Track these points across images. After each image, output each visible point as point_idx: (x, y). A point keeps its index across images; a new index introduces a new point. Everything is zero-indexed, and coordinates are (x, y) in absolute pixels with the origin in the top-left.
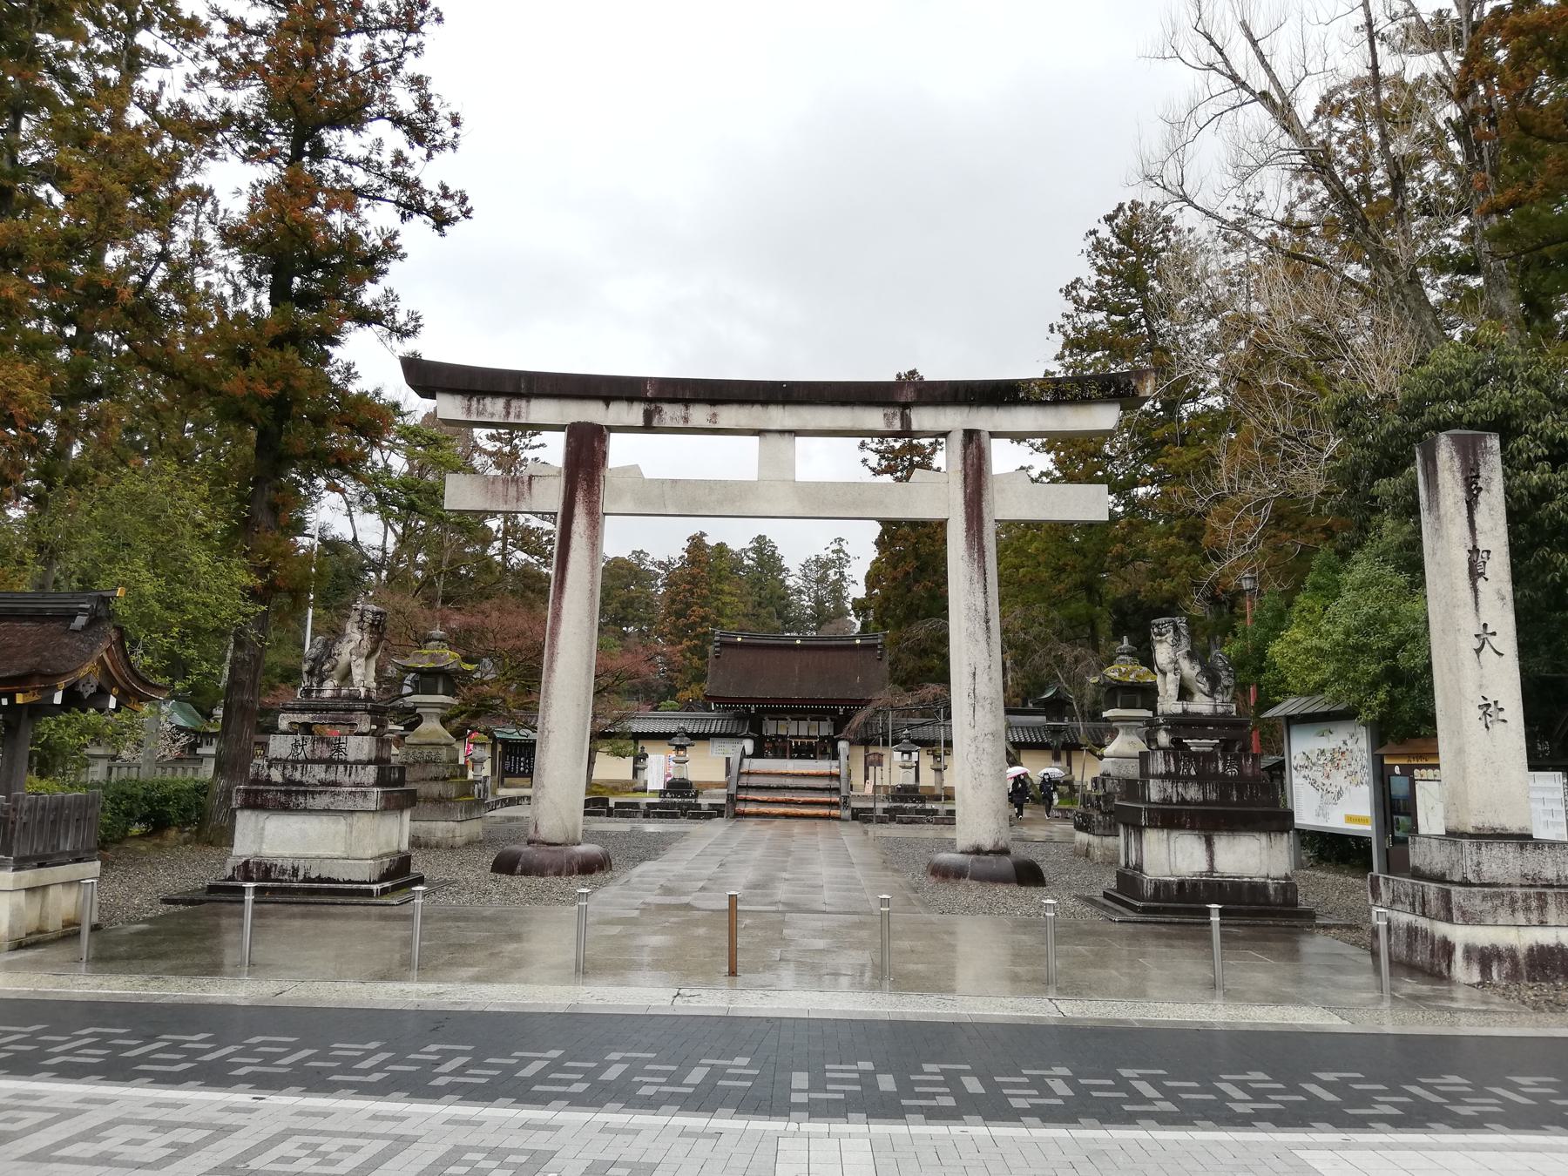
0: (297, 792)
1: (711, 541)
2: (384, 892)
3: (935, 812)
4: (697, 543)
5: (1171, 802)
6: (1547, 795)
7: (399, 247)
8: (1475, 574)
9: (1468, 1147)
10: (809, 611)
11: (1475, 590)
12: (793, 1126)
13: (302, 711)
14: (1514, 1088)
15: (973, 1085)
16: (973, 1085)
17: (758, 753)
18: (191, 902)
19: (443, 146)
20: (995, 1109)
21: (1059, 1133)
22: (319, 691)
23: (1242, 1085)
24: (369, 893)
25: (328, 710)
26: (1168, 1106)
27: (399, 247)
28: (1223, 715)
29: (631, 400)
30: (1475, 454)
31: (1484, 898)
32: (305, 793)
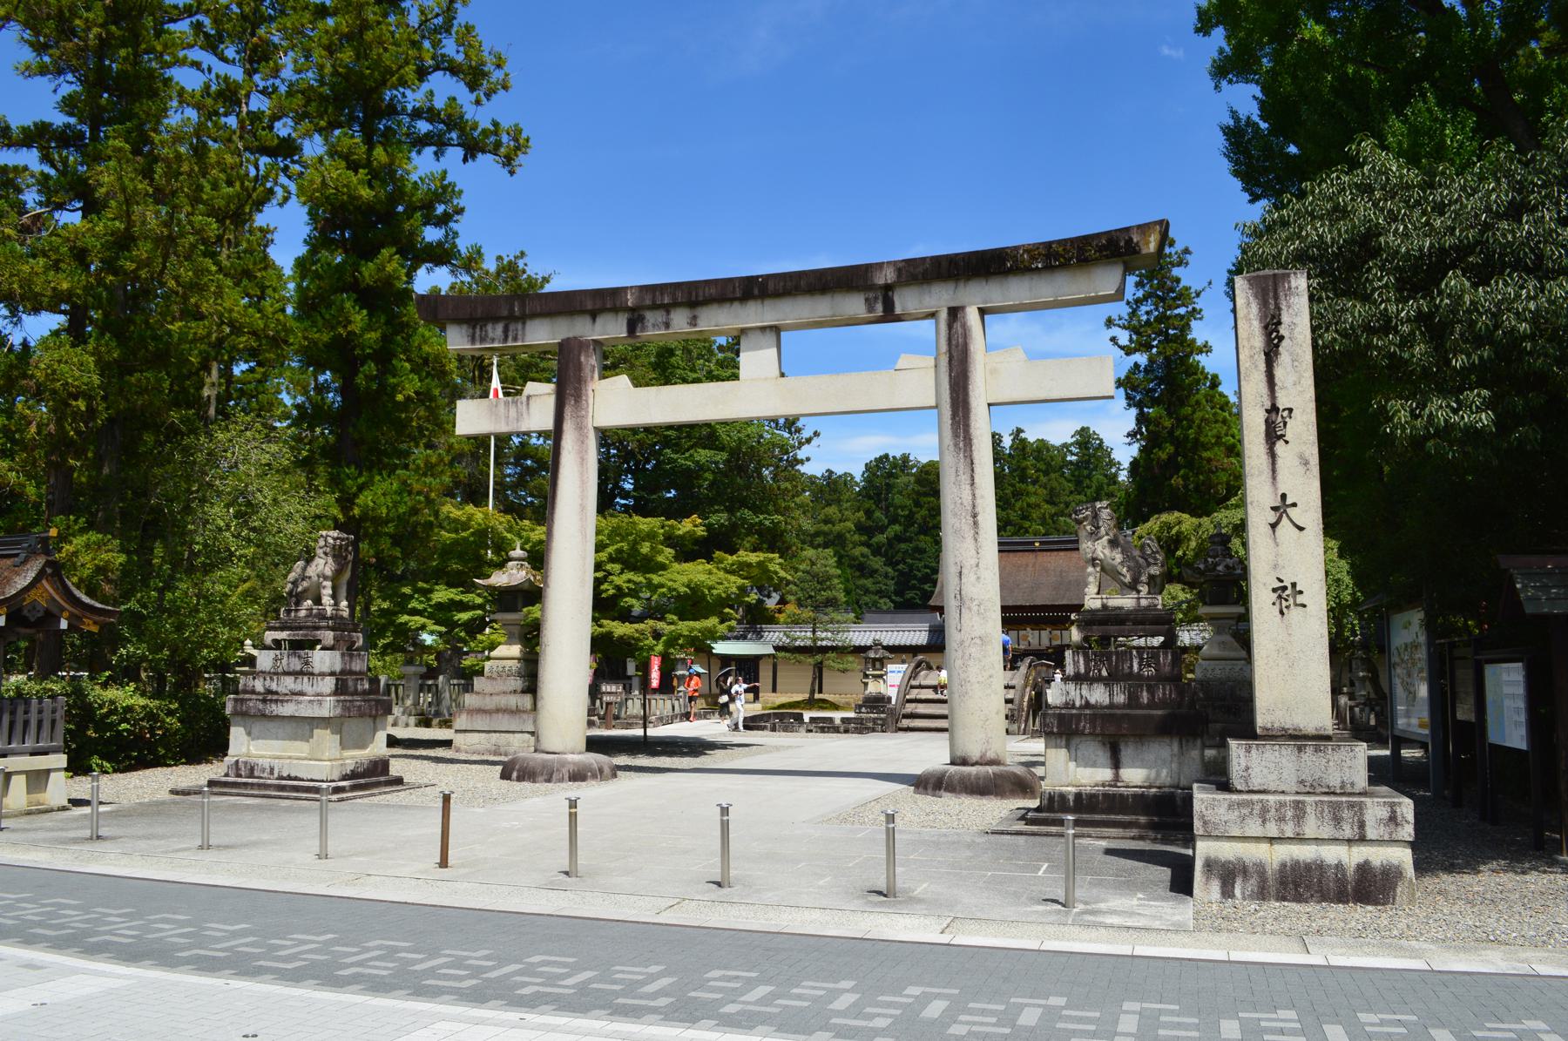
5: (1073, 706)
8: (1273, 435)
11: (1272, 455)
13: (282, 629)
25: (300, 628)
28: (1147, 608)
29: (615, 310)
30: (1276, 298)
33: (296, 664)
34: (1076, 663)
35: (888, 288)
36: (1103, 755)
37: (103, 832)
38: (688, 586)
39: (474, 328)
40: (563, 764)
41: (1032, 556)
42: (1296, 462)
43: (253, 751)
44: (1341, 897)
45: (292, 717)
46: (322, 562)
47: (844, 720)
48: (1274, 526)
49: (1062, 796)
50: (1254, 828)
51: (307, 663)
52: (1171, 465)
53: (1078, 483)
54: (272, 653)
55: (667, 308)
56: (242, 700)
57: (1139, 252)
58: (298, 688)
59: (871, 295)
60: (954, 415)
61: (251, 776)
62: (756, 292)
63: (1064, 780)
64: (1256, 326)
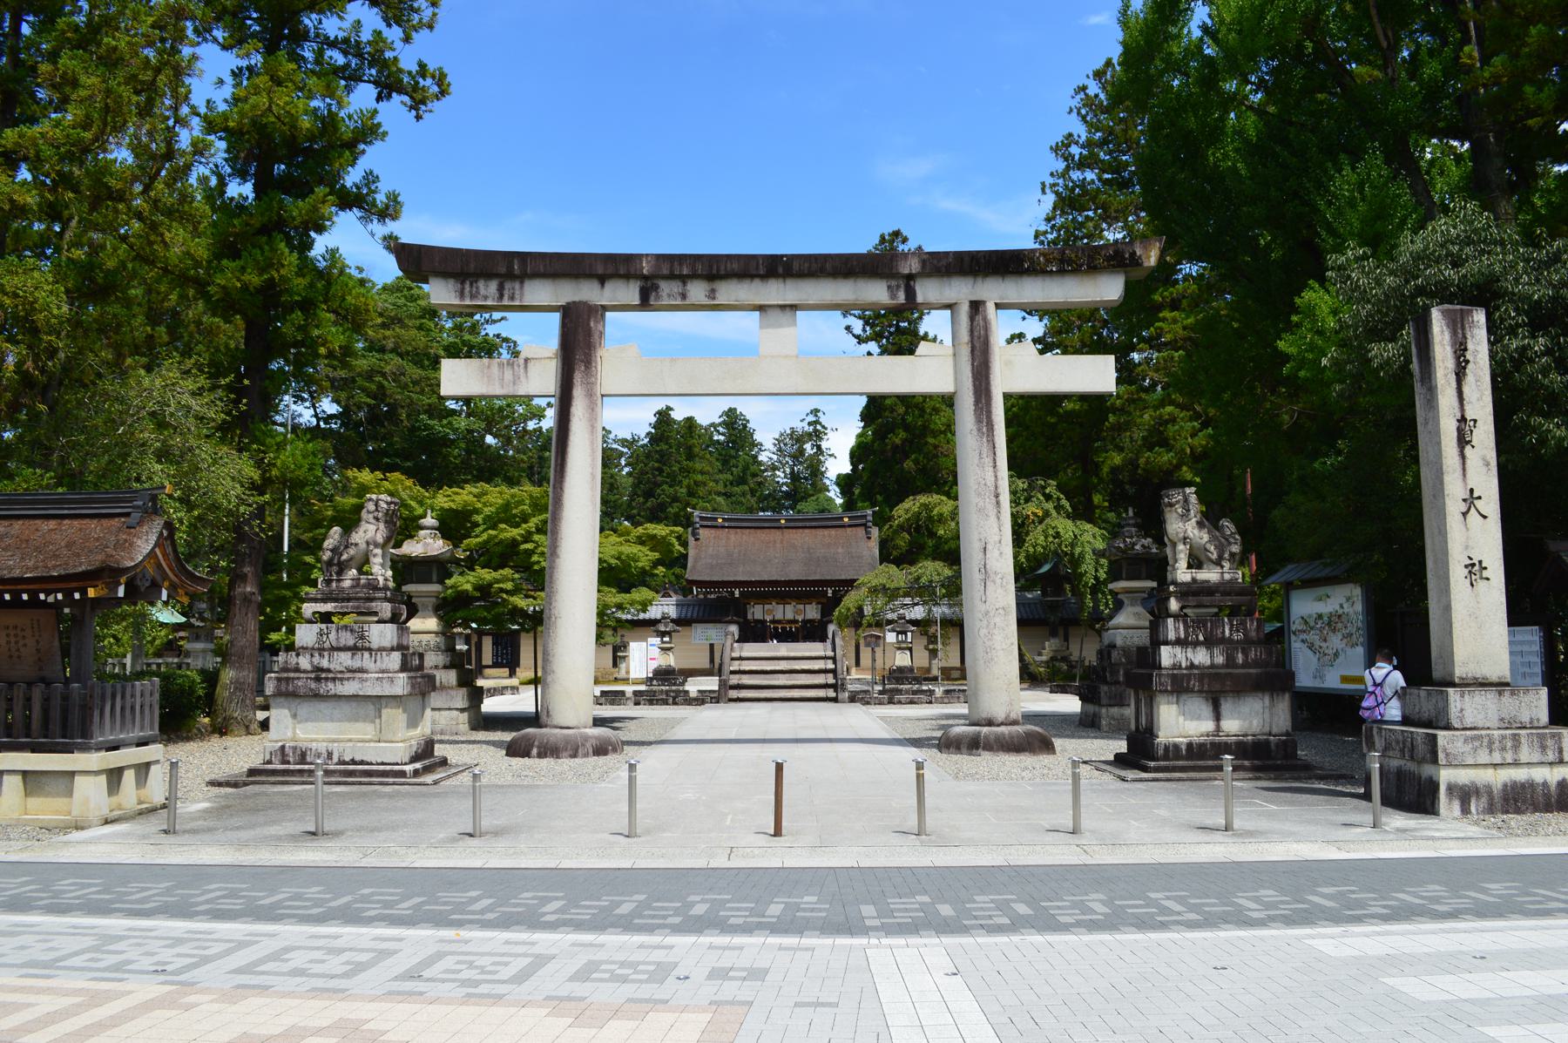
0: (327, 679)
1: (678, 415)
2: (416, 773)
3: (931, 692)
4: (663, 417)
5: (1180, 667)
6: (1526, 648)
7: (379, 125)
8: (1463, 441)
9: (1444, 931)
10: (785, 488)
11: (1463, 456)
12: (874, 941)
13: (324, 600)
14: (1484, 891)
15: (1022, 909)
16: (1022, 909)
17: (744, 638)
18: (235, 785)
19: (421, 25)
20: (1047, 923)
21: (1105, 937)
22: (339, 581)
23: (1256, 900)
24: (402, 774)
25: (349, 600)
26: (1193, 916)
27: (379, 125)
29: (627, 277)
30: (1463, 328)
31: (1466, 741)
32: (334, 679)
33: (348, 639)
34: (1177, 629)
35: (910, 278)
36: (1206, 709)
37: (328, 826)
38: (618, 558)
39: (463, 283)
40: (586, 738)
41: (778, 533)
42: (1481, 463)
43: (300, 734)
44: (1548, 808)
45: (355, 697)
46: (372, 528)
47: (636, 693)
48: (1465, 514)
49: (1176, 746)
50: (1484, 757)
51: (362, 638)
52: (903, 451)
53: (725, 462)
54: (316, 628)
55: (684, 279)
56: (288, 679)
57: (1141, 265)
58: (357, 664)
59: (894, 283)
60: (977, 402)
61: (303, 760)
62: (780, 270)
63: (1176, 733)
64: (1449, 350)
